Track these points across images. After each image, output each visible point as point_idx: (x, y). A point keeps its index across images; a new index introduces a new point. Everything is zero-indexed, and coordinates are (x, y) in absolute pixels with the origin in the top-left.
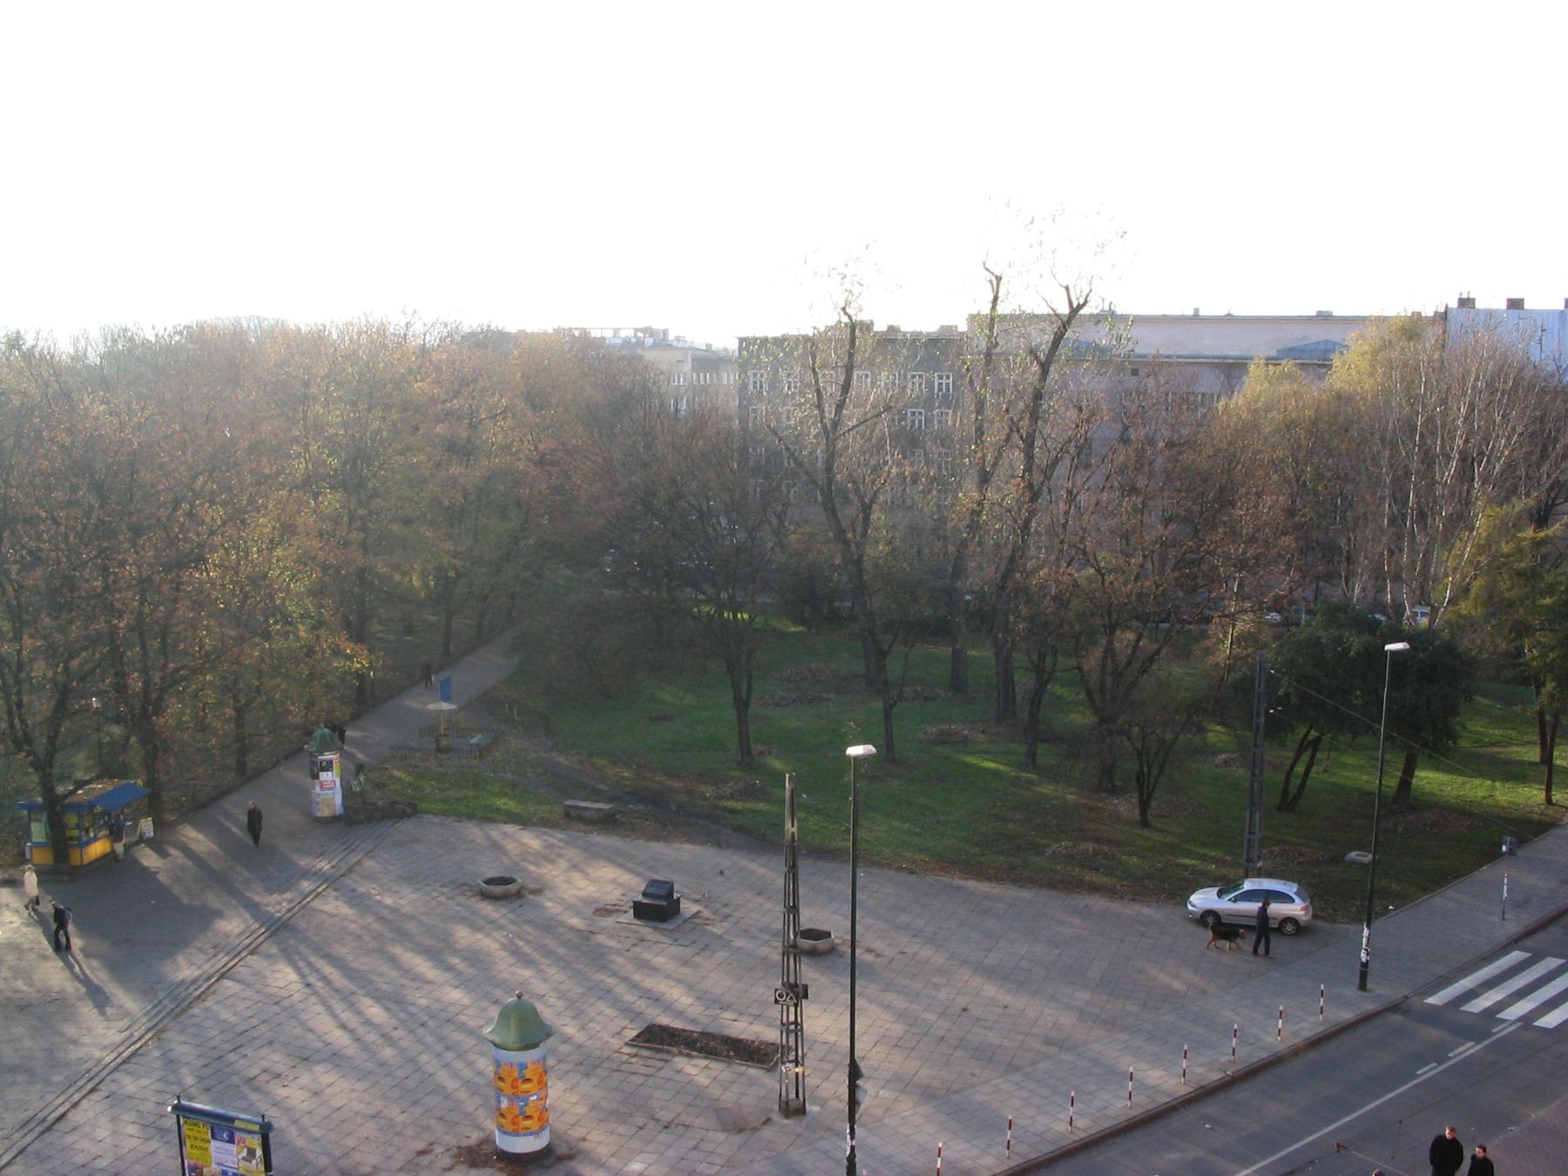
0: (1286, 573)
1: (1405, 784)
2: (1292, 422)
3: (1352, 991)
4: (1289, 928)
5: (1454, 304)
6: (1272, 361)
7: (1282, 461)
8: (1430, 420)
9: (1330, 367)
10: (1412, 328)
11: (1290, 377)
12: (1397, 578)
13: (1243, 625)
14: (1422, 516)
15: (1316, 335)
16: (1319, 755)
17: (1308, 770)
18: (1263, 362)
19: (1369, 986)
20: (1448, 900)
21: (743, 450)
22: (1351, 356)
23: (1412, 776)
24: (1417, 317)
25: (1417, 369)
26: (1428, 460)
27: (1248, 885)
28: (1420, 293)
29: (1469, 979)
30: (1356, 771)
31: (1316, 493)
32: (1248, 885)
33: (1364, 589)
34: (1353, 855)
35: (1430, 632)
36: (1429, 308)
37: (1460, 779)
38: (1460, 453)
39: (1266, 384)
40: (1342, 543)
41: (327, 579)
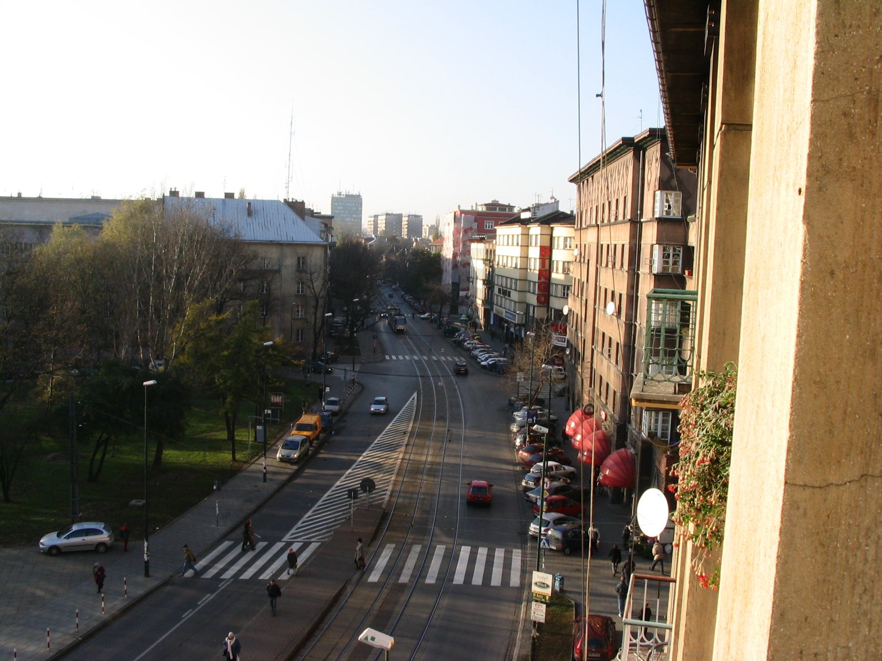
0: (81, 346)
1: (158, 458)
2: (80, 259)
3: (141, 578)
4: (102, 549)
5: (167, 194)
6: (65, 224)
7: (75, 282)
8: (158, 257)
9: (101, 228)
10: (146, 206)
11: (76, 233)
12: (145, 346)
13: (58, 377)
14: (157, 310)
15: (91, 210)
16: (109, 448)
17: (103, 457)
18: (61, 225)
19: (151, 573)
20: (187, 519)
21: (205, 230)
22: (113, 223)
23: (161, 454)
24: (148, 200)
25: (151, 229)
26: (159, 279)
27: (75, 528)
28: (150, 187)
29: (706, 361)
30: (131, 455)
31: (96, 300)
32: (75, 528)
33: (126, 353)
34: (133, 502)
35: (166, 374)
36: (156, 196)
37: (187, 453)
38: (176, 275)
39: (64, 238)
40: (113, 327)
41: (259, 260)
